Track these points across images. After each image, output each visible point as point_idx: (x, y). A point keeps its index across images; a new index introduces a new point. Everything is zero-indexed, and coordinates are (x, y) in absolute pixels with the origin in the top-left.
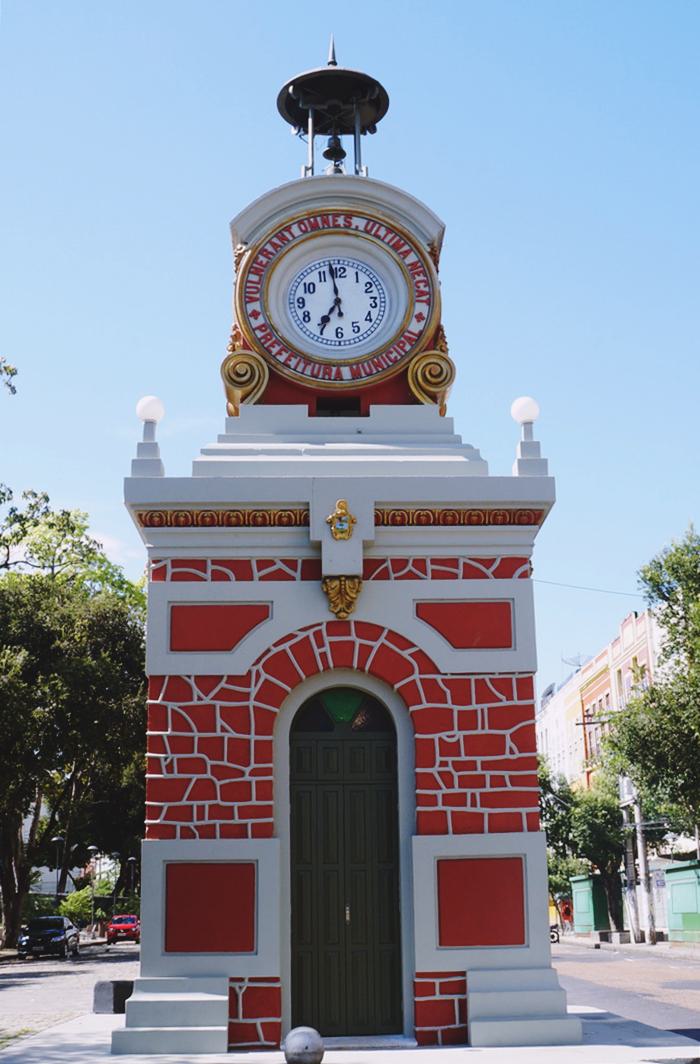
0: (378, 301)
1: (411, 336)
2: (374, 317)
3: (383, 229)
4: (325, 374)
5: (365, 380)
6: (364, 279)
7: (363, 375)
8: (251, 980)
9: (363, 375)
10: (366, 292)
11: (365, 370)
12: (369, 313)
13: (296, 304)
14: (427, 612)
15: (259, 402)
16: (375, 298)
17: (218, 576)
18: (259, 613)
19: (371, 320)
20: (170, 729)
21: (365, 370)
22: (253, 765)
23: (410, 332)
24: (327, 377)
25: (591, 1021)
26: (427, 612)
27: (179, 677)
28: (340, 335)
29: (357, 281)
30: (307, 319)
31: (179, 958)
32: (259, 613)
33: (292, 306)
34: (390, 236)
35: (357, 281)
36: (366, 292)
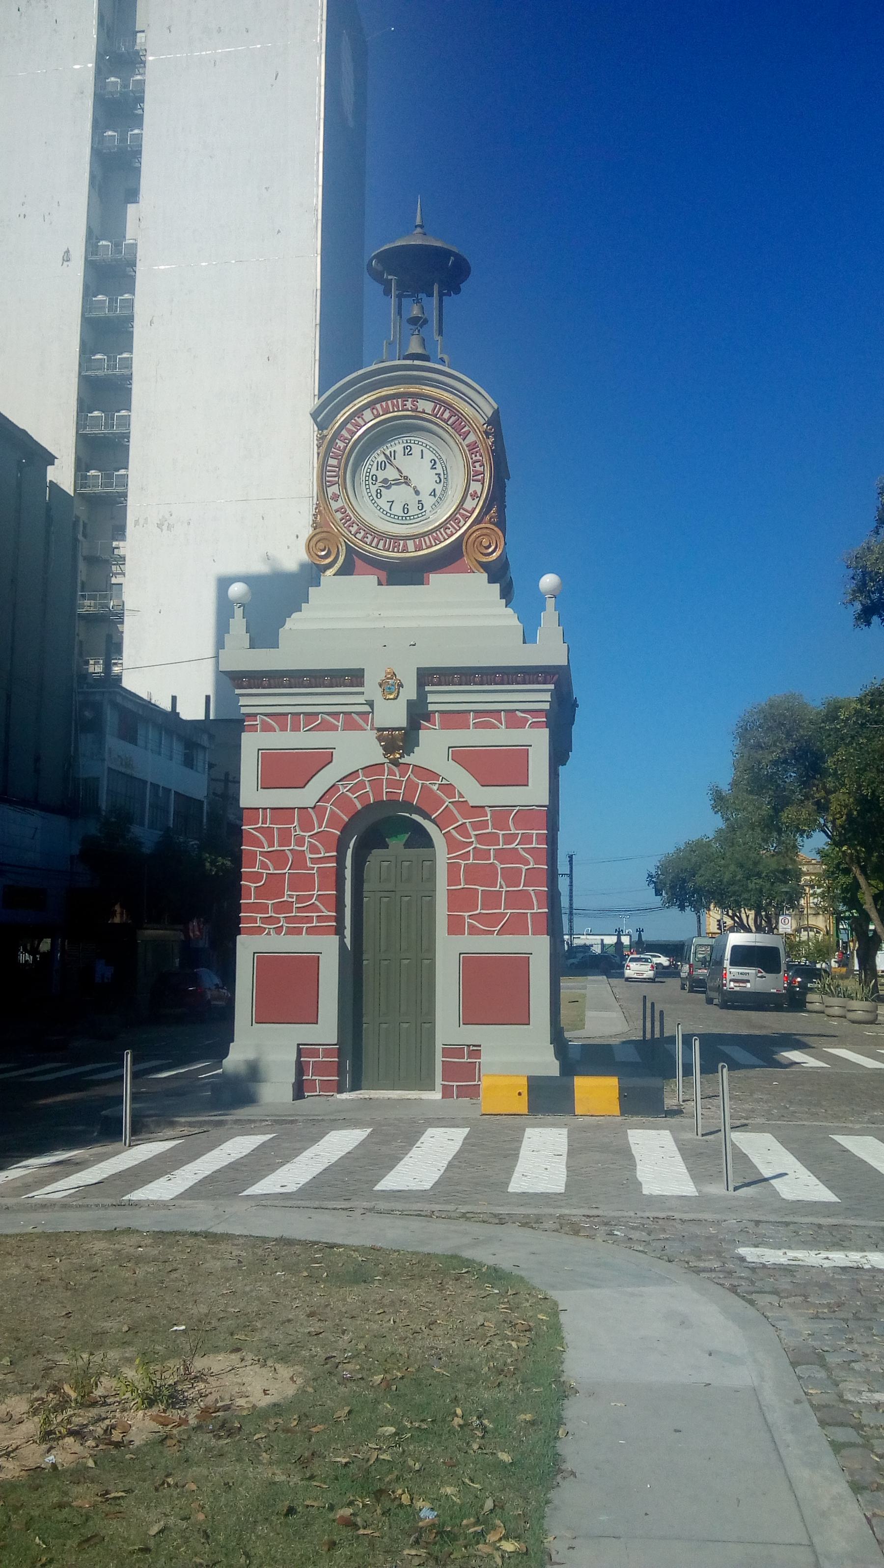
0: (442, 477)
2: (438, 493)
3: (448, 411)
4: (435, 539)
6: (429, 456)
10: (432, 468)
11: (426, 544)
13: (371, 481)
14: (461, 756)
16: (439, 474)
17: (267, 728)
18: (324, 758)
19: (435, 495)
21: (426, 544)
23: (464, 509)
25: (77, 1189)
26: (461, 756)
27: (455, 788)
28: (406, 510)
29: (422, 458)
31: (672, 939)
32: (324, 758)
33: (367, 483)
34: (453, 419)
35: (422, 458)
36: (432, 468)
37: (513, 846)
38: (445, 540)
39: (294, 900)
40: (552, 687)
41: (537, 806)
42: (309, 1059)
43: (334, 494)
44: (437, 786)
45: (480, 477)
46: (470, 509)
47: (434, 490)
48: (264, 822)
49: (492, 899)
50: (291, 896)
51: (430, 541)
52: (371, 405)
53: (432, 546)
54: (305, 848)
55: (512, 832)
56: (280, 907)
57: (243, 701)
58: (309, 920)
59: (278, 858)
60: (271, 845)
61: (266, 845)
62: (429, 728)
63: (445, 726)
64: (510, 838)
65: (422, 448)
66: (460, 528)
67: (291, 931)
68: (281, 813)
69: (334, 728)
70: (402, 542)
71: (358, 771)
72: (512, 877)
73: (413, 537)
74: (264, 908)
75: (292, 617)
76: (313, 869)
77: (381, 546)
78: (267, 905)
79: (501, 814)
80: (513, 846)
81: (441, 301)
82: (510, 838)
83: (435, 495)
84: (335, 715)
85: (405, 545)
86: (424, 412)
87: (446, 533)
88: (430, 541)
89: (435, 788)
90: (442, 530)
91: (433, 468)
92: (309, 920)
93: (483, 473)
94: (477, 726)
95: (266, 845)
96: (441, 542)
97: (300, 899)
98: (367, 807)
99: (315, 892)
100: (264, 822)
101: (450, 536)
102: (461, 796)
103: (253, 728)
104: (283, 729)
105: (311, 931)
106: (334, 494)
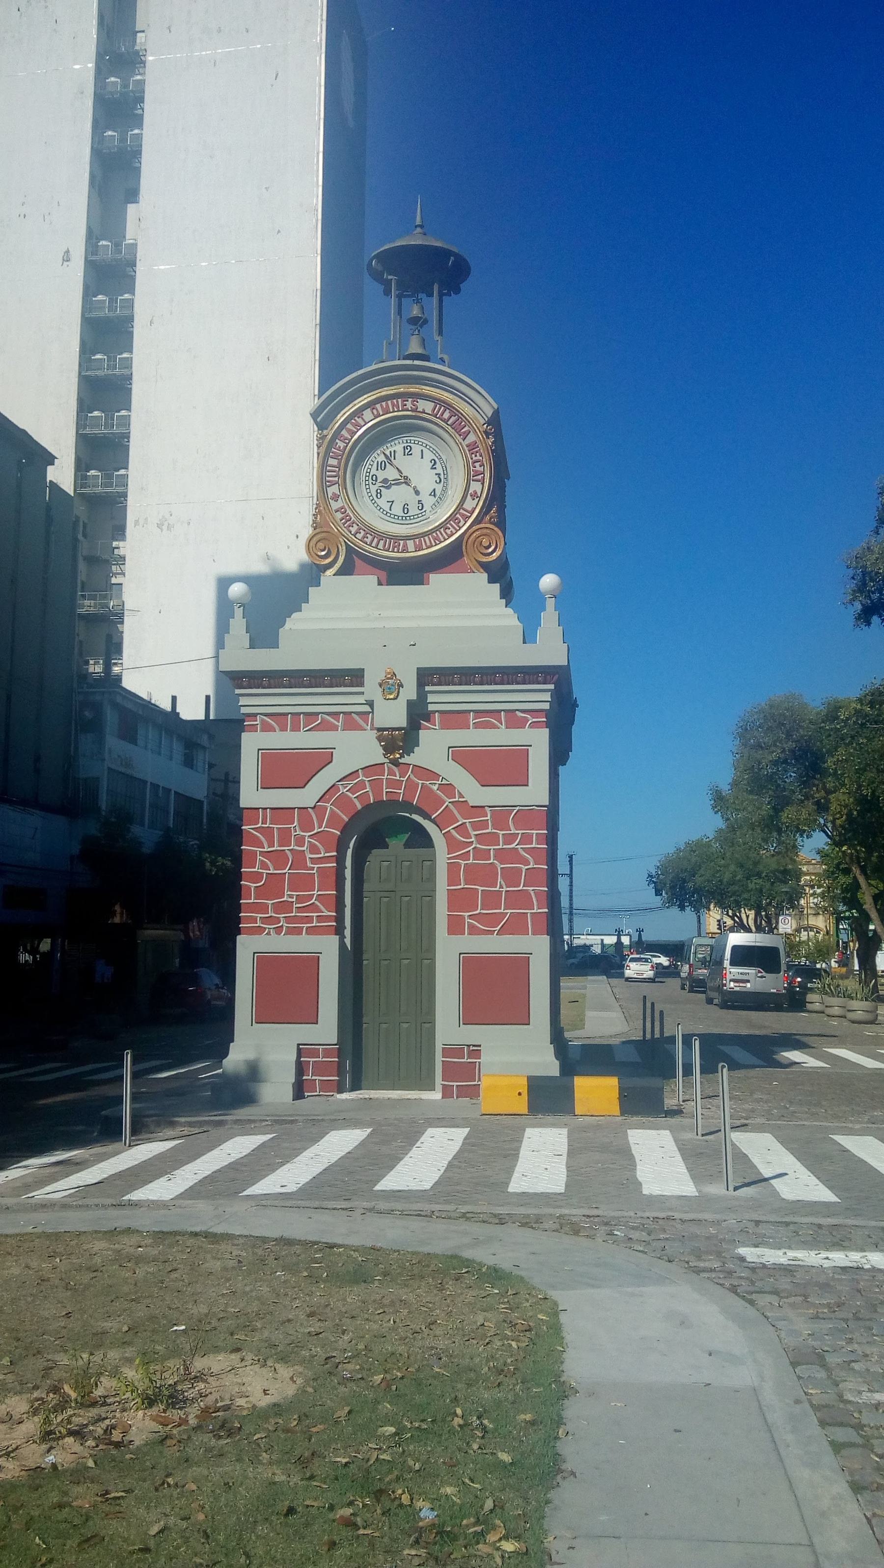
1: (465, 513)
2: (438, 493)
5: (379, 452)
6: (429, 455)
7: (424, 547)
8: (492, 932)
9: (424, 547)
10: (432, 468)
12: (434, 490)
13: (371, 481)
14: (460, 756)
15: (338, 573)
16: (439, 474)
18: (324, 758)
19: (435, 495)
20: (532, 864)
22: (524, 868)
24: (396, 550)
26: (460, 756)
29: (422, 458)
30: (379, 491)
32: (324, 758)
33: (367, 483)
35: (422, 458)
36: (432, 468)
37: (513, 846)
38: (445, 540)
39: (294, 900)
40: (552, 687)
41: (537, 806)
42: (309, 1059)
43: (334, 494)
44: (437, 786)
45: (480, 477)
46: (470, 509)
47: (434, 490)
48: (264, 822)
49: (492, 899)
50: (291, 896)
51: (430, 541)
52: (371, 405)
53: (432, 546)
54: (305, 848)
55: (512, 832)
56: (279, 908)
57: (243, 701)
58: (309, 919)
59: (278, 858)
60: (271, 845)
61: (266, 845)
62: (429, 728)
63: (445, 726)
64: (510, 838)
65: (422, 448)
66: (460, 528)
67: (291, 931)
68: (281, 813)
69: (334, 728)
70: (402, 542)
71: (259, 808)
72: (511, 877)
73: (412, 537)
74: (263, 908)
75: (292, 617)
76: (313, 869)
77: (381, 546)
78: (267, 905)
79: (501, 814)
80: (513, 846)
81: (441, 301)
82: (510, 838)
83: (435, 495)
84: (335, 715)
85: (405, 545)
86: (424, 412)
87: (446, 533)
88: (430, 541)
89: (435, 788)
90: (442, 530)
91: (433, 468)
92: (309, 919)
93: (483, 473)
94: (477, 726)
95: (266, 845)
96: (441, 542)
97: (299, 899)
98: (367, 807)
99: (315, 892)
100: (264, 822)
101: (450, 537)
102: (461, 796)
103: (253, 728)
104: (283, 729)
105: (311, 931)
106: (334, 494)
